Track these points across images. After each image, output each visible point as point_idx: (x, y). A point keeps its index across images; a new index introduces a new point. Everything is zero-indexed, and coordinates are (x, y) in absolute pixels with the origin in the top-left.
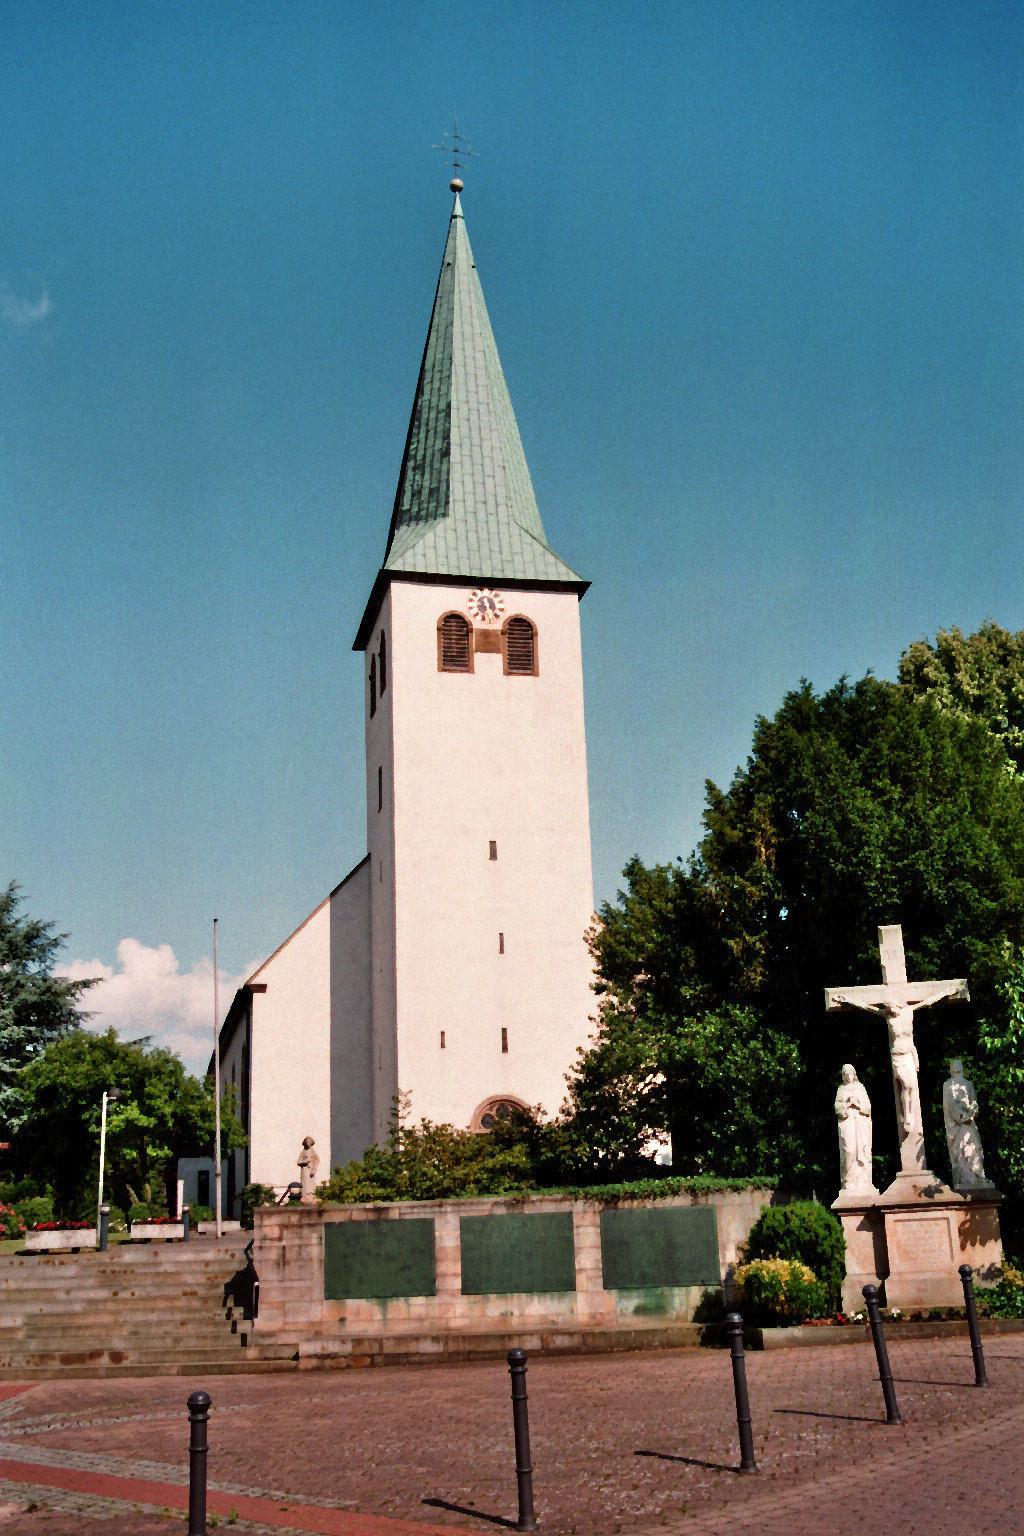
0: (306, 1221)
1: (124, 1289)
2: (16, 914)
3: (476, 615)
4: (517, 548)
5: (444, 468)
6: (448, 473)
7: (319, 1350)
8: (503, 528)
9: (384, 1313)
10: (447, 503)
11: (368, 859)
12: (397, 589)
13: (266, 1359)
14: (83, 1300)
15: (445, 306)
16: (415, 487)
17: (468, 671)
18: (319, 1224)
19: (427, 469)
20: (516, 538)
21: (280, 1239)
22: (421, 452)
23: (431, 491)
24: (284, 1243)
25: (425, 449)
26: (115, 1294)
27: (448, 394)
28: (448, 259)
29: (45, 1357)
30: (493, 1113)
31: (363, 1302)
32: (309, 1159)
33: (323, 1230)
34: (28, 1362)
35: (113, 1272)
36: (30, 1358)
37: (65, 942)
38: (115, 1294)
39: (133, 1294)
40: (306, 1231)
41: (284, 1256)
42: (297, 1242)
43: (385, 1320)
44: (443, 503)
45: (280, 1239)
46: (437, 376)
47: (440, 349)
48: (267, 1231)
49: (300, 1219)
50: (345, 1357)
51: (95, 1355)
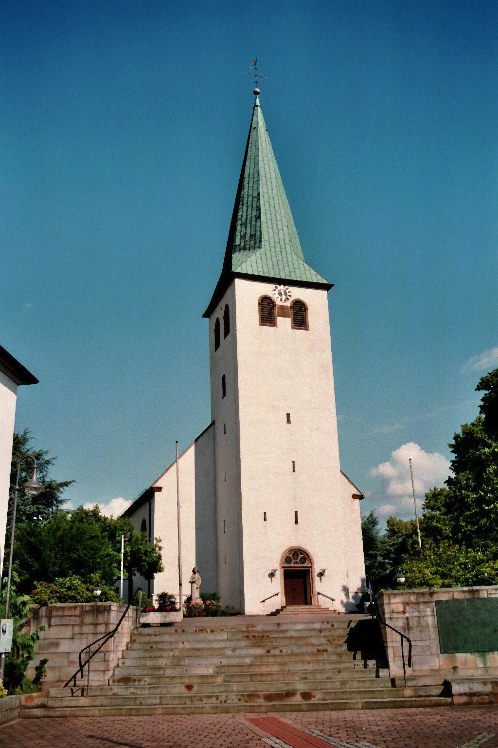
0: (421, 600)
1: (274, 648)
2: (27, 447)
3: (277, 298)
4: (296, 265)
5: (258, 224)
6: (260, 227)
7: (467, 690)
8: (289, 256)
9: (485, 662)
10: (261, 241)
11: (213, 423)
12: (238, 282)
13: (419, 696)
14: (251, 656)
15: (254, 148)
16: (242, 234)
17: (274, 326)
18: (430, 602)
19: (249, 225)
20: (295, 262)
21: (404, 612)
22: (244, 217)
23: (251, 236)
24: (407, 615)
25: (247, 215)
26: (268, 651)
27: (258, 188)
28: (254, 125)
29: (252, 696)
30: (291, 556)
31: (468, 655)
32: (196, 579)
33: (434, 605)
34: (239, 700)
35: (254, 637)
36: (241, 697)
37: (54, 461)
38: (268, 651)
39: (281, 651)
40: (422, 607)
41: (408, 624)
42: (416, 614)
43: (486, 668)
44: (258, 241)
45: (404, 612)
46: (251, 180)
47: (252, 167)
48: (393, 606)
49: (417, 599)
50: (487, 695)
51: (290, 694)
